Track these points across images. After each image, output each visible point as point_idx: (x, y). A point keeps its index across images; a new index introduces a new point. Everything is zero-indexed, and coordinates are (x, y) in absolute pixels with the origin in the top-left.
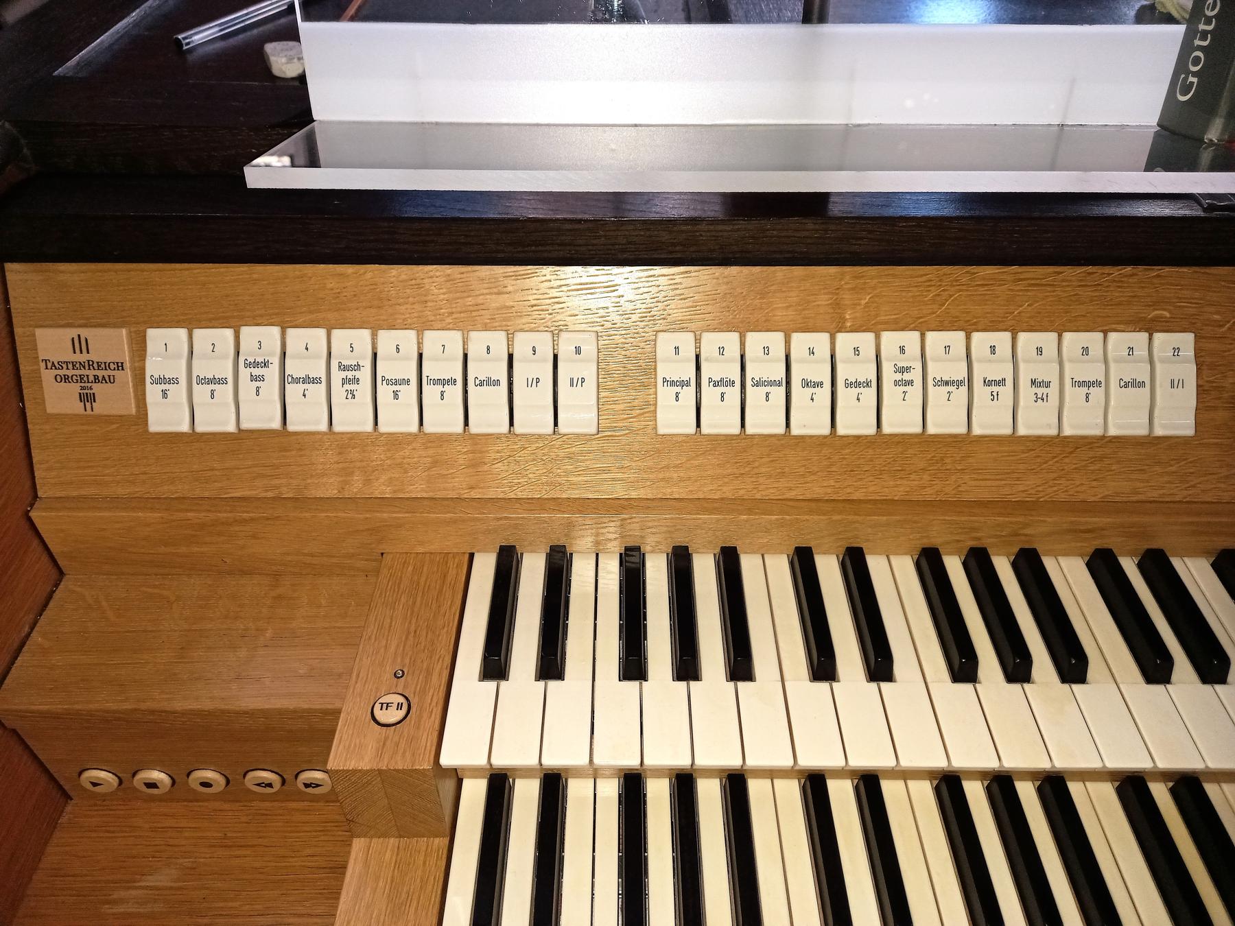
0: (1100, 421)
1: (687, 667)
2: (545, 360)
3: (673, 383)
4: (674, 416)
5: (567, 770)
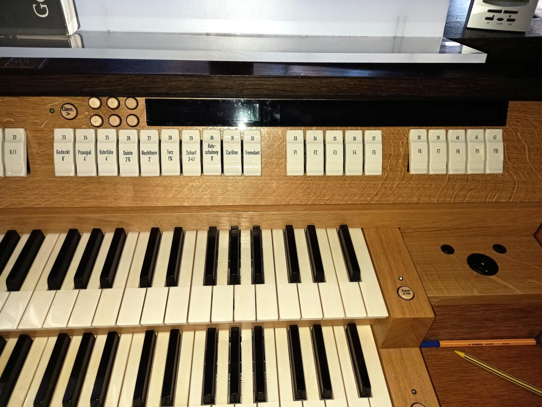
0: (426, 167)
1: (234, 279)
2: (237, 142)
3: (83, 153)
4: (294, 167)
5: (181, 326)
